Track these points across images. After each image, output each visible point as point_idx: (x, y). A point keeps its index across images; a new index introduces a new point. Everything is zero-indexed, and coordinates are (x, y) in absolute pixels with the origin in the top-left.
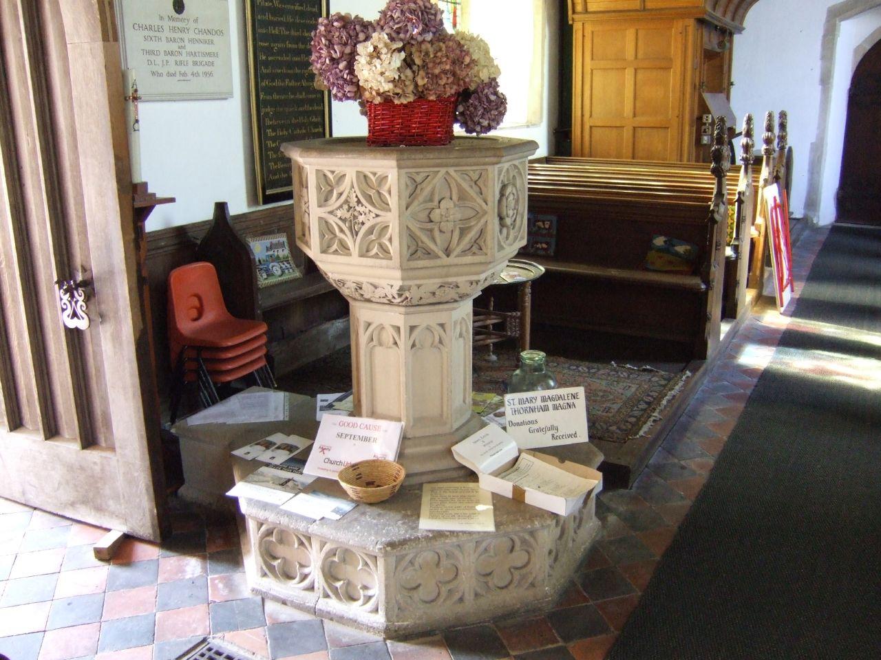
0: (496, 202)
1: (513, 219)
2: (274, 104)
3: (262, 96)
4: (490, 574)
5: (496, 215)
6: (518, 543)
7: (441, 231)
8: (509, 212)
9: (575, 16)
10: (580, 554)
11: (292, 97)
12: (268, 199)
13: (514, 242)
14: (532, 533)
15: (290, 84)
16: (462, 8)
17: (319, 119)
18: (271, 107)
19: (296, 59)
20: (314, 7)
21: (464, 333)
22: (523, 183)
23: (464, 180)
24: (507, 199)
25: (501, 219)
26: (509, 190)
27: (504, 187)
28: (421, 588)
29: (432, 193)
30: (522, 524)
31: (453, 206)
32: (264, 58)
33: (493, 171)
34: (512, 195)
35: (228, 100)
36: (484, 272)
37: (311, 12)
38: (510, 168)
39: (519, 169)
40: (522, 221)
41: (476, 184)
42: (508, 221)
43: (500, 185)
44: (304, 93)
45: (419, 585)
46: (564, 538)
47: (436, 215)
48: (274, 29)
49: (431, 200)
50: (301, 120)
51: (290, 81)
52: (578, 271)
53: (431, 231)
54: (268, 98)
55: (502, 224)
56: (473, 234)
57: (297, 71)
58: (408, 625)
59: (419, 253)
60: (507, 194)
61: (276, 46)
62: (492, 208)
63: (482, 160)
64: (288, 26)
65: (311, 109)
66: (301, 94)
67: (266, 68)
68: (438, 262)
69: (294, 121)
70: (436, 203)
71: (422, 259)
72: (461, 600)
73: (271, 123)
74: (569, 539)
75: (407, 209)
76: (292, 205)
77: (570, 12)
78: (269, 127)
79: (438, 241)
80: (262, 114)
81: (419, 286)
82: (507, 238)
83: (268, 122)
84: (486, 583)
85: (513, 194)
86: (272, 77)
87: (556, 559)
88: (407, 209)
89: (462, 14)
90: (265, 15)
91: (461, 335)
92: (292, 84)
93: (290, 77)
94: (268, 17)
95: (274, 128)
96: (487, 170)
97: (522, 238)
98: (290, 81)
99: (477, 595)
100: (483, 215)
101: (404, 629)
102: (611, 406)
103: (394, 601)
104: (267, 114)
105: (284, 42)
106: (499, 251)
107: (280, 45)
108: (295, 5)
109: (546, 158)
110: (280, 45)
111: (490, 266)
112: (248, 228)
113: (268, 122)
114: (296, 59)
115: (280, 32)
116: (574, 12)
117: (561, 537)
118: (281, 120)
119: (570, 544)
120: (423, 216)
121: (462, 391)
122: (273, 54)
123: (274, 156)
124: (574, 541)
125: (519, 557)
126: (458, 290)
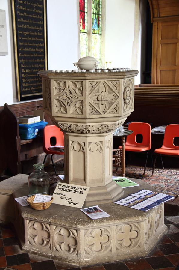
0: (123, 94)
1: (129, 100)
2: (24, 58)
3: (20, 55)
4: (122, 240)
5: (123, 99)
6: (133, 227)
7: (101, 104)
8: (127, 98)
9: (154, 19)
10: (159, 237)
11: (32, 56)
12: (22, 99)
13: (130, 109)
14: (138, 223)
15: (31, 50)
16: (102, 17)
17: (43, 66)
18: (23, 60)
19: (34, 39)
20: (41, 16)
21: (109, 146)
22: (133, 87)
23: (111, 85)
24: (127, 92)
25: (124, 100)
26: (127, 89)
27: (125, 88)
28: (95, 245)
29: (99, 90)
30: (134, 219)
31: (106, 94)
32: (20, 38)
33: (122, 81)
34: (128, 91)
35: (6, 56)
36: (118, 120)
37: (40, 19)
38: (128, 81)
39: (131, 81)
40: (132, 102)
41: (115, 86)
42: (127, 101)
43: (124, 87)
44: (37, 54)
45: (94, 244)
46: (152, 229)
47: (100, 98)
48: (24, 26)
49: (98, 92)
50: (36, 66)
51: (31, 49)
52: (163, 268)
53: (98, 104)
54: (23, 56)
55: (125, 103)
56: (114, 106)
57: (34, 45)
58: (89, 261)
59: (93, 112)
60: (127, 91)
61: (26, 33)
62: (121, 96)
63: (117, 77)
64: (30, 25)
65: (40, 61)
66: (36, 54)
67: (21, 42)
68: (100, 116)
69: (33, 66)
70: (100, 93)
71: (94, 115)
72: (111, 251)
73: (24, 66)
74: (154, 231)
75: (89, 95)
76: (42, 95)
77: (152, 17)
78: (23, 68)
79: (100, 108)
80: (20, 62)
81: (93, 125)
82: (127, 108)
83: (22, 66)
84: (121, 244)
85: (129, 91)
86: (24, 47)
87: (149, 237)
88: (89, 95)
89: (102, 19)
90: (21, 19)
91: (108, 147)
92: (32, 50)
93: (32, 47)
94: (22, 20)
95: (25, 69)
96: (119, 81)
97: (132, 109)
98: (31, 49)
99: (117, 249)
100: (118, 98)
101: (88, 262)
102: (169, 184)
103: (84, 250)
104: (22, 63)
105: (28, 32)
106: (123, 112)
107: (27, 33)
108: (33, 15)
109: (140, 85)
110: (27, 33)
111: (120, 118)
112: (14, 111)
113: (22, 66)
114: (34, 39)
115: (27, 27)
116: (153, 17)
117: (150, 229)
118: (27, 65)
119: (154, 233)
120: (95, 98)
121: (109, 170)
122: (24, 37)
123: (25, 81)
124: (156, 232)
125: (134, 234)
126: (108, 127)
